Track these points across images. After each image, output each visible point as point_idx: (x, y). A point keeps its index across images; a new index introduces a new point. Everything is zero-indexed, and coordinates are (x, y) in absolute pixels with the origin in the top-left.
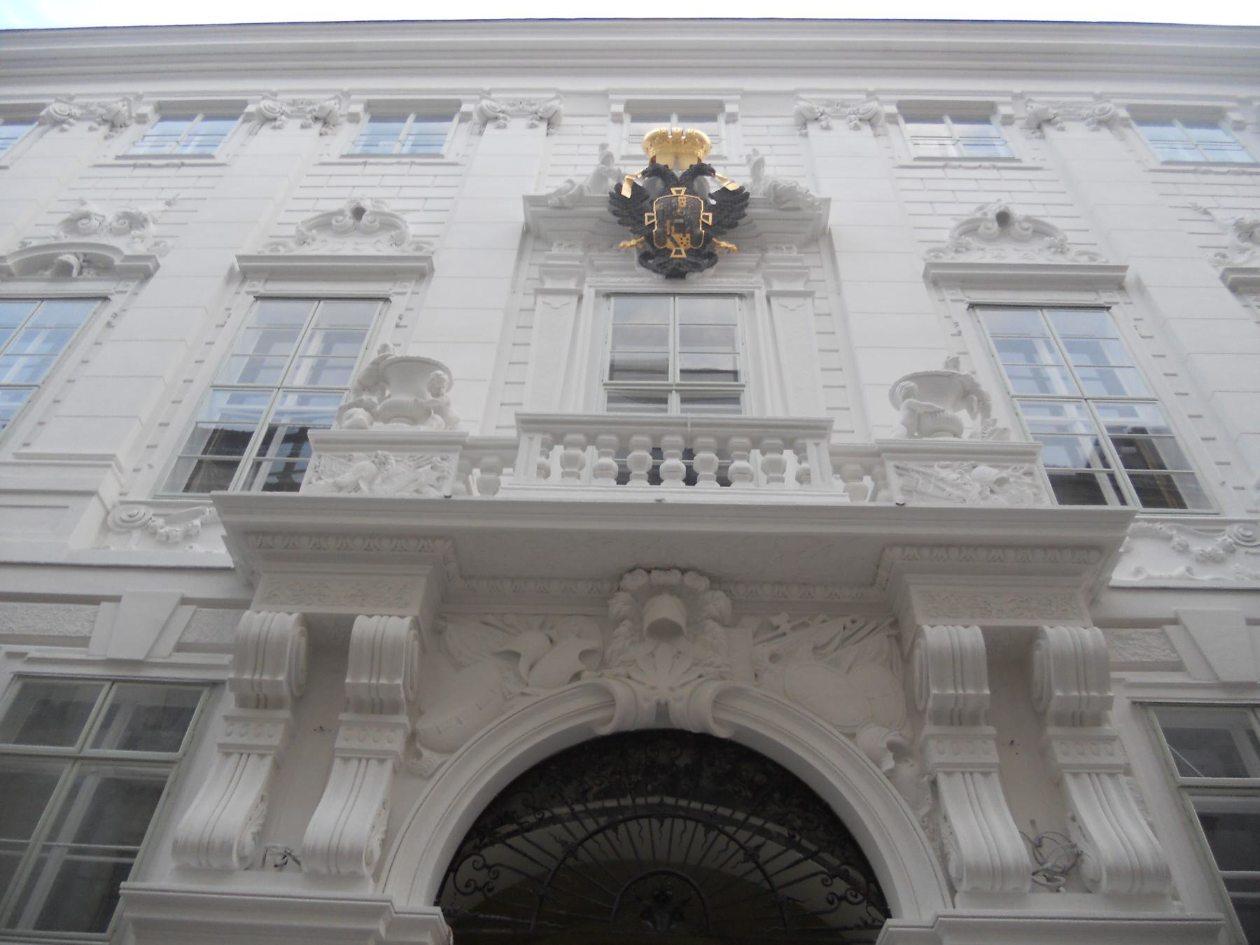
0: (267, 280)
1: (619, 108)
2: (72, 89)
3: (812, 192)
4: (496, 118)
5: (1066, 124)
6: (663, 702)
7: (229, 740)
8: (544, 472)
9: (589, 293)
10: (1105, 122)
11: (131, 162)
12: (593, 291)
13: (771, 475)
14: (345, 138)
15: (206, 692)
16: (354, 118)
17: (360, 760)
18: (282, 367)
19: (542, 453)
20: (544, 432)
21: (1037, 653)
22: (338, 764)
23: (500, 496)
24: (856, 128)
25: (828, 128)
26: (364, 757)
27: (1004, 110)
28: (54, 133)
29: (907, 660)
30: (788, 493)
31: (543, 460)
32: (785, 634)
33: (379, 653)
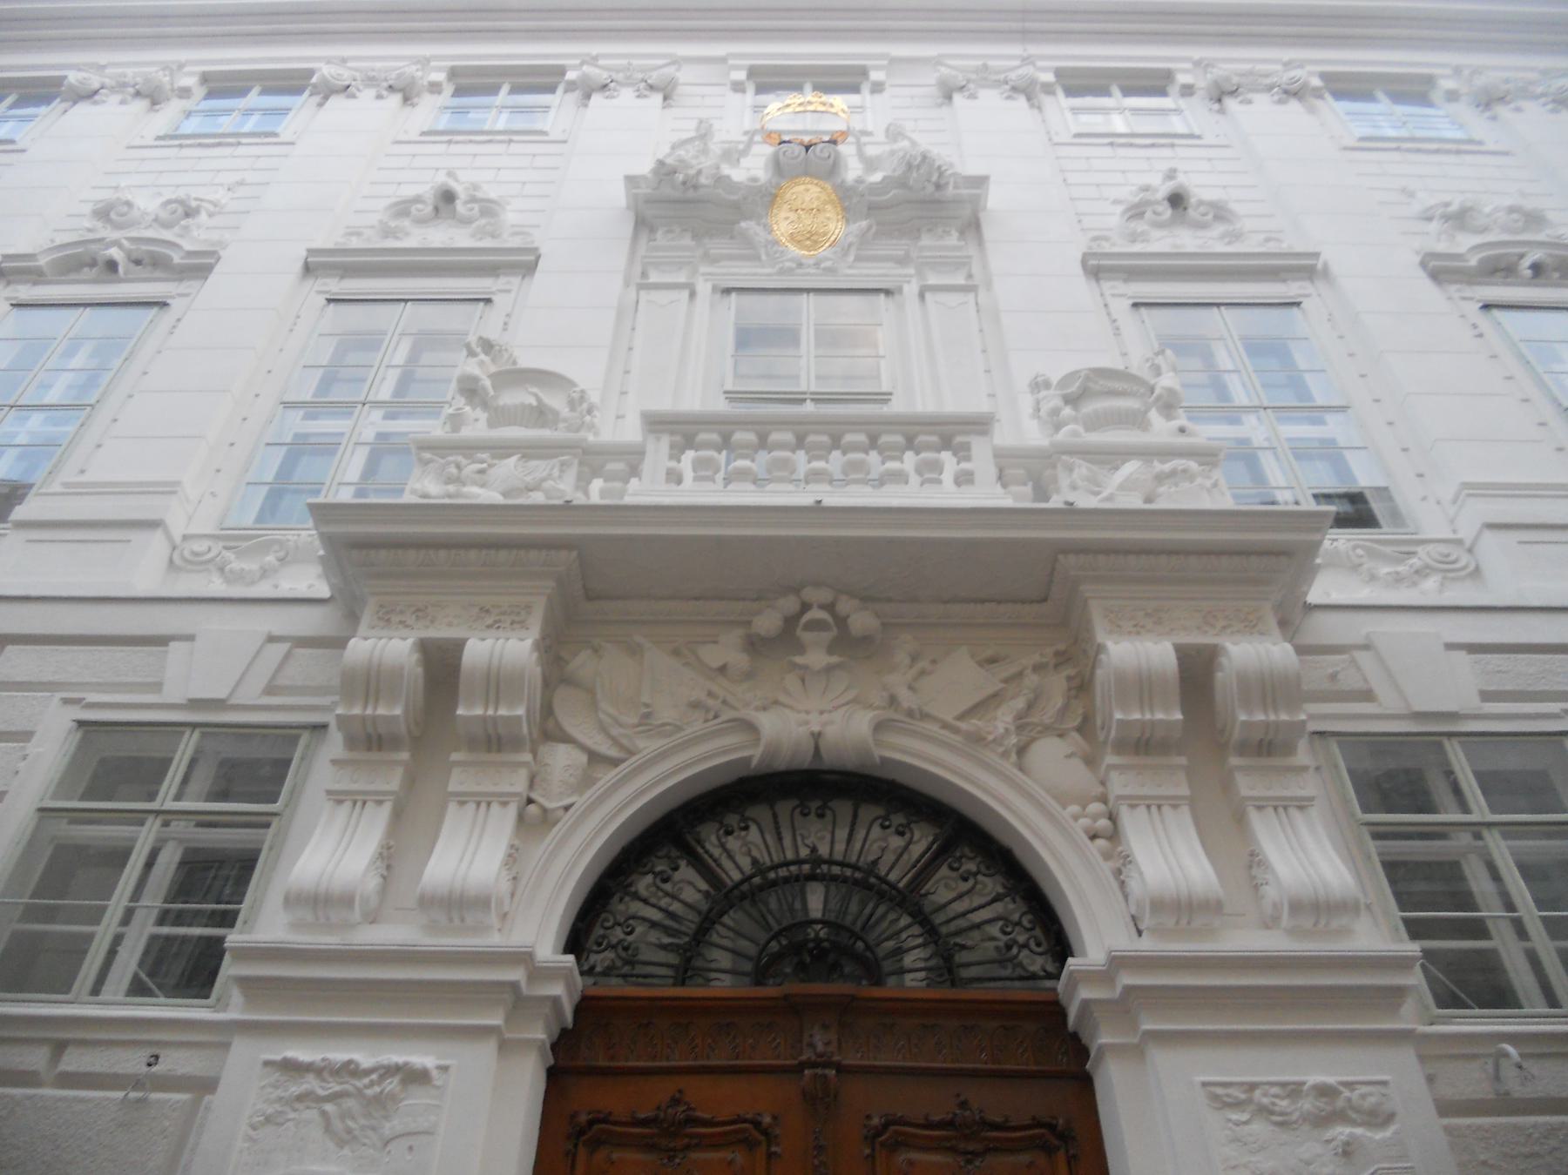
0: (342, 277)
1: (741, 75)
2: (101, 57)
5: (1250, 96)
7: (337, 787)
8: (675, 477)
9: (704, 288)
10: (1294, 93)
11: (177, 142)
12: (709, 286)
13: (927, 476)
14: (429, 111)
15: (305, 737)
16: (435, 88)
17: (478, 804)
18: (364, 380)
19: (671, 457)
20: (672, 433)
21: (1219, 675)
22: (452, 807)
23: (628, 500)
26: (483, 801)
27: (1182, 79)
28: (83, 109)
30: (946, 495)
31: (673, 464)
33: (496, 683)
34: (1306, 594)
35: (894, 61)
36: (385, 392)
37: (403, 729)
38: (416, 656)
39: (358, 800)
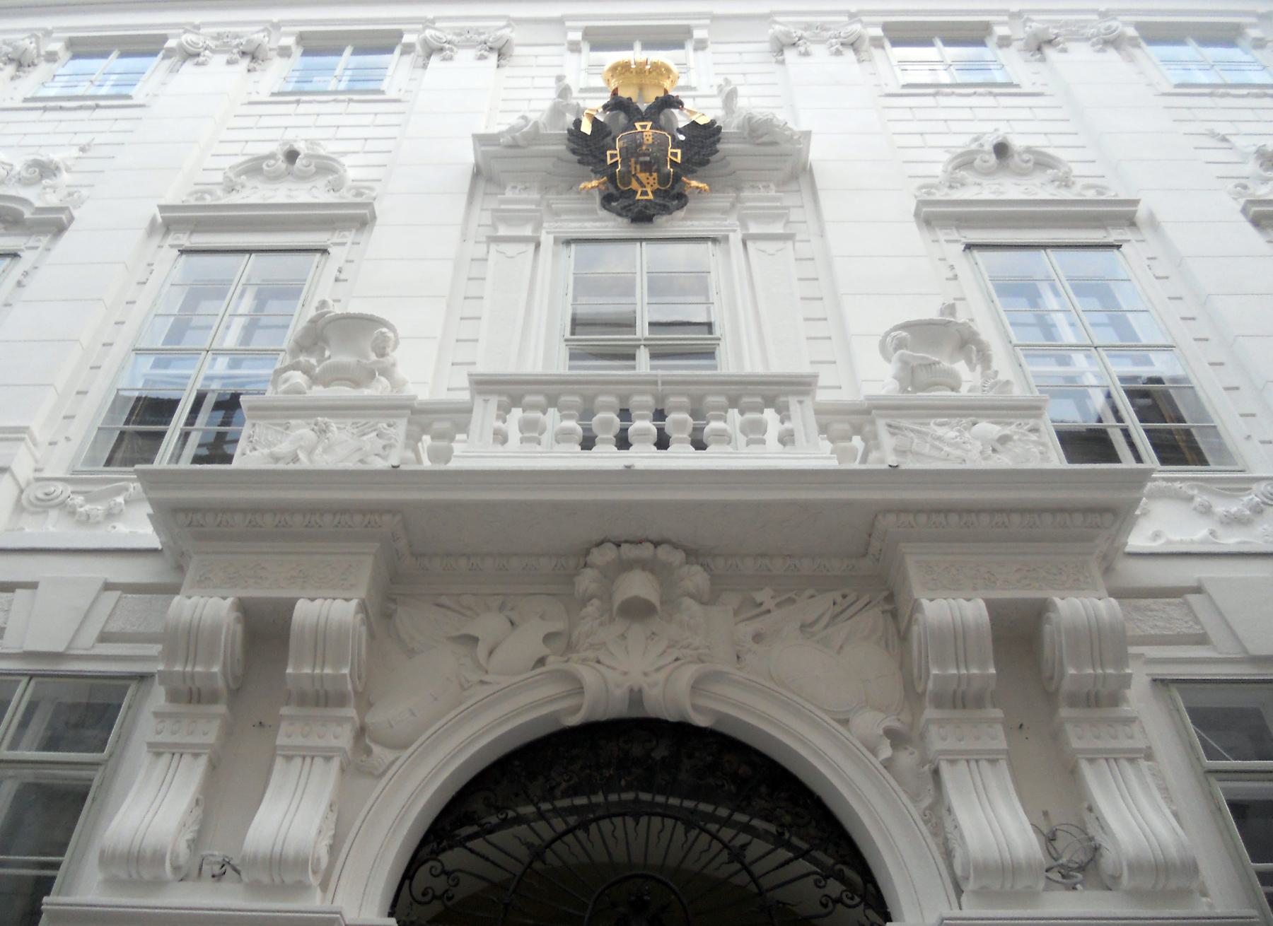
0: (192, 232)
3: (790, 125)
4: (442, 49)
7: (159, 739)
9: (547, 240)
12: (551, 237)
14: (276, 73)
15: (133, 686)
18: (210, 328)
19: (498, 417)
20: (500, 393)
24: (838, 53)
25: (806, 54)
27: (1000, 31)
31: (499, 424)
32: (769, 611)
34: (1126, 544)
35: (715, 18)
36: (231, 339)
37: (220, 684)
38: (234, 615)
39: (177, 751)
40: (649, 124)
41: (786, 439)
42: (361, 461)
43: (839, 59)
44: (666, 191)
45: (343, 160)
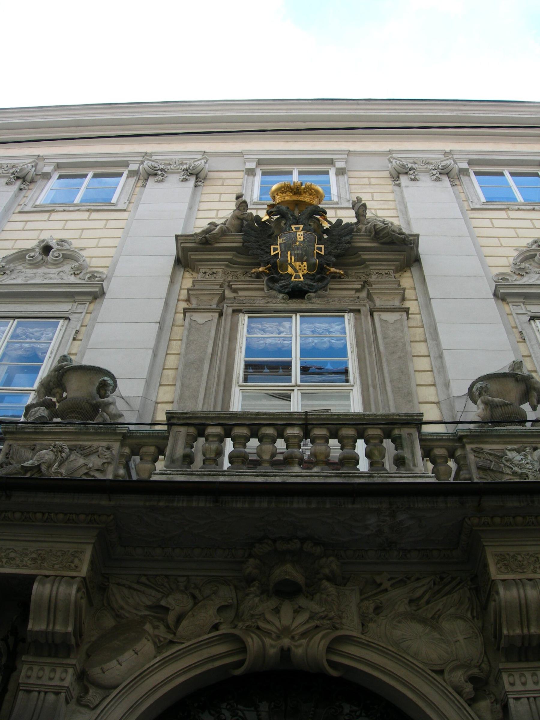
3: (404, 231)
4: (156, 175)
6: (286, 647)
17: (39, 692)
24: (438, 180)
25: (415, 180)
29: (485, 608)
32: (386, 590)
40: (301, 227)
41: (400, 462)
42: (86, 474)
43: (438, 184)
44: (313, 275)
45: (82, 253)
